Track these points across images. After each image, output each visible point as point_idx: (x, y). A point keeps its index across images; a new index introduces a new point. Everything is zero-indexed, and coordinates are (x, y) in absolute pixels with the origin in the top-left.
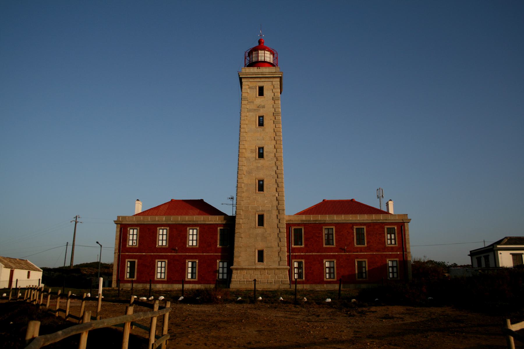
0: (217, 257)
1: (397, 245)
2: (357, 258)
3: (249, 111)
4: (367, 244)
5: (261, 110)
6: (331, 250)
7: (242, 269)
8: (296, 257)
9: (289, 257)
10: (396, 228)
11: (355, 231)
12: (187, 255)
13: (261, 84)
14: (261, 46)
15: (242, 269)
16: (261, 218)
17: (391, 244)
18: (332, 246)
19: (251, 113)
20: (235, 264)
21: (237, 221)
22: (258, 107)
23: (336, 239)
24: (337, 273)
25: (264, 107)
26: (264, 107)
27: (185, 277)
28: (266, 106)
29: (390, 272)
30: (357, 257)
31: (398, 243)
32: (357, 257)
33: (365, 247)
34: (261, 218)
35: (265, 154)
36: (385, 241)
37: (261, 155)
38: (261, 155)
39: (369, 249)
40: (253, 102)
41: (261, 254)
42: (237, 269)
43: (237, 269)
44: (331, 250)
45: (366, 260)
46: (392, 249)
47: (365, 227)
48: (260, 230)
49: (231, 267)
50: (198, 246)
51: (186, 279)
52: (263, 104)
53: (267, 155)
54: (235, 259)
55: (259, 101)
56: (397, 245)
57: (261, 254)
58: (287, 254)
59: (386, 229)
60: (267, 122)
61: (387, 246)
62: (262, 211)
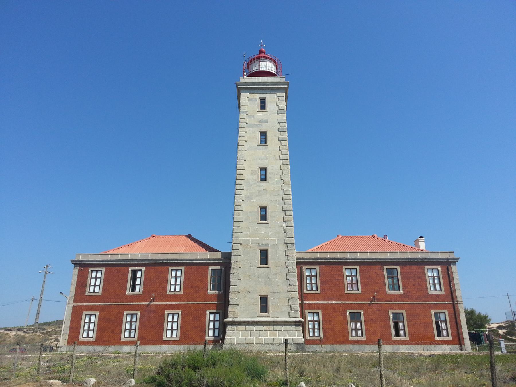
0: (209, 307)
1: (443, 292)
2: (392, 309)
3: (250, 126)
4: (404, 290)
5: (263, 124)
6: (436, 307)
7: (240, 323)
8: (310, 306)
9: (302, 305)
10: (440, 269)
11: (385, 273)
12: (166, 305)
13: (263, 96)
14: (261, 56)
15: (240, 323)
16: (264, 253)
17: (435, 290)
18: (357, 292)
19: (251, 129)
20: (230, 315)
21: (233, 258)
22: (260, 122)
23: (361, 283)
24: (367, 330)
25: (266, 121)
26: (266, 121)
27: (162, 336)
28: (269, 121)
29: (443, 329)
30: (392, 307)
31: (445, 290)
32: (392, 307)
33: (401, 295)
34: (264, 253)
35: (269, 176)
36: (427, 287)
37: (264, 178)
38: (264, 178)
39: (405, 296)
40: (253, 116)
41: (264, 300)
42: (233, 323)
43: (233, 323)
44: (436, 307)
45: (404, 312)
46: (437, 297)
47: (398, 267)
48: (263, 270)
49: (226, 320)
50: (181, 292)
51: (165, 339)
52: (265, 118)
53: (271, 177)
54: (230, 308)
55: (261, 114)
56: (443, 292)
57: (264, 300)
58: (299, 302)
59: (385, 271)
60: (269, 136)
61: (430, 292)
62: (266, 245)
